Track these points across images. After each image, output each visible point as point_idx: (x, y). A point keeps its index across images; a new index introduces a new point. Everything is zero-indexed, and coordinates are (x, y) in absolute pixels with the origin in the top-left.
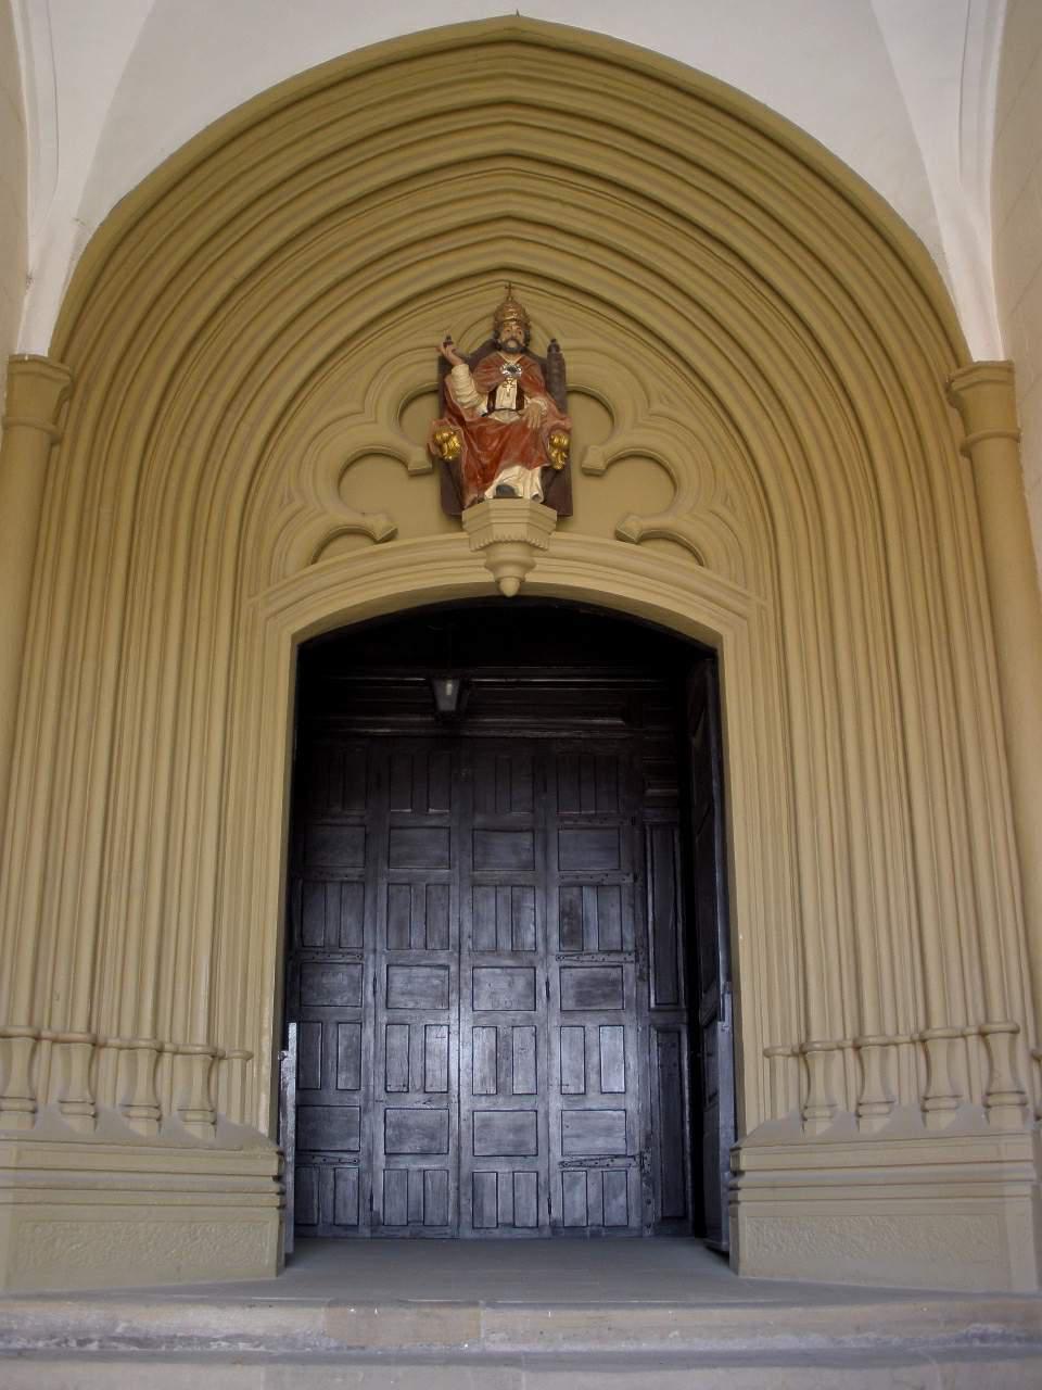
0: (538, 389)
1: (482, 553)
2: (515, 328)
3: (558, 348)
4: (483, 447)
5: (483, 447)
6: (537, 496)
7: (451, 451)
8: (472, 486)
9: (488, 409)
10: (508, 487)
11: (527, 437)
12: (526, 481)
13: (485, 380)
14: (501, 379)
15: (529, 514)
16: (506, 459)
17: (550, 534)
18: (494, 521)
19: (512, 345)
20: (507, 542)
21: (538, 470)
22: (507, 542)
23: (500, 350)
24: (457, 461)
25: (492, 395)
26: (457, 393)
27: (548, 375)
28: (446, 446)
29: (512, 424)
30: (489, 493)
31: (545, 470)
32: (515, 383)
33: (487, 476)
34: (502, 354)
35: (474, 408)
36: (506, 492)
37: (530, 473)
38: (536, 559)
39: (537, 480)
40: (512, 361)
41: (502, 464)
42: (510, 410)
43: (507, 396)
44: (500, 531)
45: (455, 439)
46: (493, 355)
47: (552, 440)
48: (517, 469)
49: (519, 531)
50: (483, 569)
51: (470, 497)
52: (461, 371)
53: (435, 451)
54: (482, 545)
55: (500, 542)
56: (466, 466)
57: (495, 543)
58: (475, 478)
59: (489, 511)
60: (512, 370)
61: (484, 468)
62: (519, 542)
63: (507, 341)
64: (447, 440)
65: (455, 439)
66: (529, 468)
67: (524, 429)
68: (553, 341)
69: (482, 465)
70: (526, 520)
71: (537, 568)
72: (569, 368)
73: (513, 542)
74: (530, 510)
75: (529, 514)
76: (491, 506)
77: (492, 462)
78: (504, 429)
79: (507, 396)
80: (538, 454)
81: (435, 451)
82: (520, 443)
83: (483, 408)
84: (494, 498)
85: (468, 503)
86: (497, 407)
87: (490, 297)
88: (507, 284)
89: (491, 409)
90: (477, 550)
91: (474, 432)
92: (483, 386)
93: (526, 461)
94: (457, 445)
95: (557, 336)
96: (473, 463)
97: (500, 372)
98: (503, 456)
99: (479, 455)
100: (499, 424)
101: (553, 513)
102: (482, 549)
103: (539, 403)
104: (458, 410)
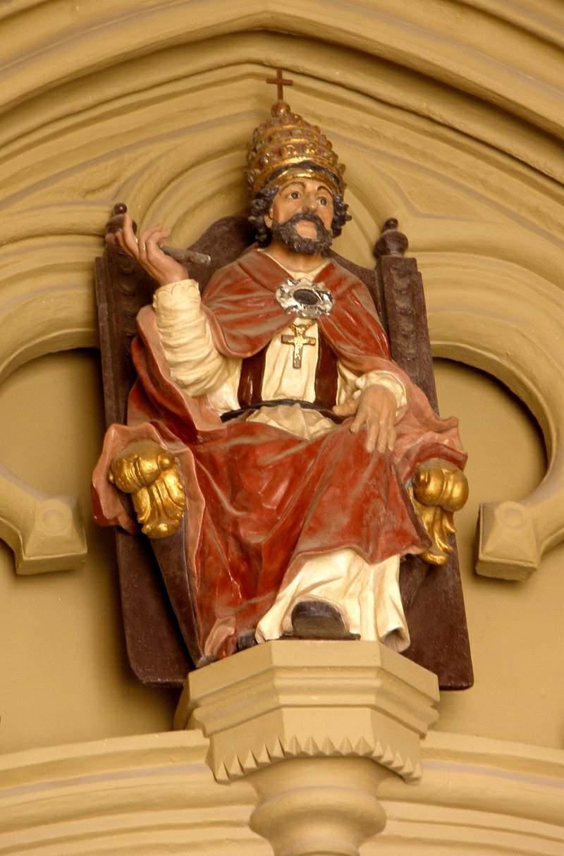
0: (374, 350)
1: (245, 788)
2: (312, 186)
3: (402, 242)
4: (248, 501)
5: (248, 501)
6: (396, 633)
7: (159, 511)
8: (221, 608)
9: (242, 402)
10: (327, 608)
11: (366, 474)
12: (361, 588)
13: (240, 322)
14: (280, 321)
15: (377, 683)
16: (312, 531)
17: (423, 736)
18: (284, 699)
19: (306, 231)
20: (320, 757)
21: (392, 565)
22: (320, 757)
23: (266, 244)
24: (175, 540)
25: (253, 367)
26: (168, 355)
27: (385, 307)
28: (144, 500)
29: (318, 442)
30: (272, 623)
31: (407, 564)
32: (313, 332)
33: (259, 575)
34: (276, 256)
35: (201, 398)
36: (316, 621)
37: (372, 571)
38: (392, 808)
39: (393, 591)
40: (304, 274)
41: (305, 545)
42: (305, 405)
43: (291, 371)
44: (302, 728)
45: (171, 480)
46: (251, 257)
47: (419, 485)
48: (342, 562)
49: (355, 729)
50: (247, 833)
51: (222, 631)
52: (180, 299)
53: (111, 509)
54: (250, 764)
55: (303, 757)
56: (201, 553)
57: (289, 759)
58: (225, 583)
59: (271, 671)
60: (305, 297)
61: (248, 554)
62: (353, 757)
63: (295, 219)
64: (148, 482)
65: (171, 480)
66: (372, 560)
67: (360, 456)
68: (391, 224)
69: (242, 546)
70: (371, 699)
71: (391, 828)
72: (431, 296)
73: (337, 757)
74: (381, 671)
75: (377, 683)
76: (277, 660)
77: (272, 544)
78: (301, 458)
79: (291, 371)
80: (395, 521)
81: (111, 509)
82: (337, 490)
83: (227, 397)
84: (285, 636)
85: (207, 652)
86: (267, 393)
87: (223, 107)
88: (274, 73)
89: (250, 399)
90: (232, 779)
91: (226, 463)
92: (234, 338)
93: (362, 538)
94: (176, 494)
95: (399, 213)
96: (217, 544)
97: (277, 303)
98: (308, 522)
99: (235, 523)
100: (289, 441)
101: (428, 680)
102: (247, 775)
103: (388, 384)
104: (178, 403)
